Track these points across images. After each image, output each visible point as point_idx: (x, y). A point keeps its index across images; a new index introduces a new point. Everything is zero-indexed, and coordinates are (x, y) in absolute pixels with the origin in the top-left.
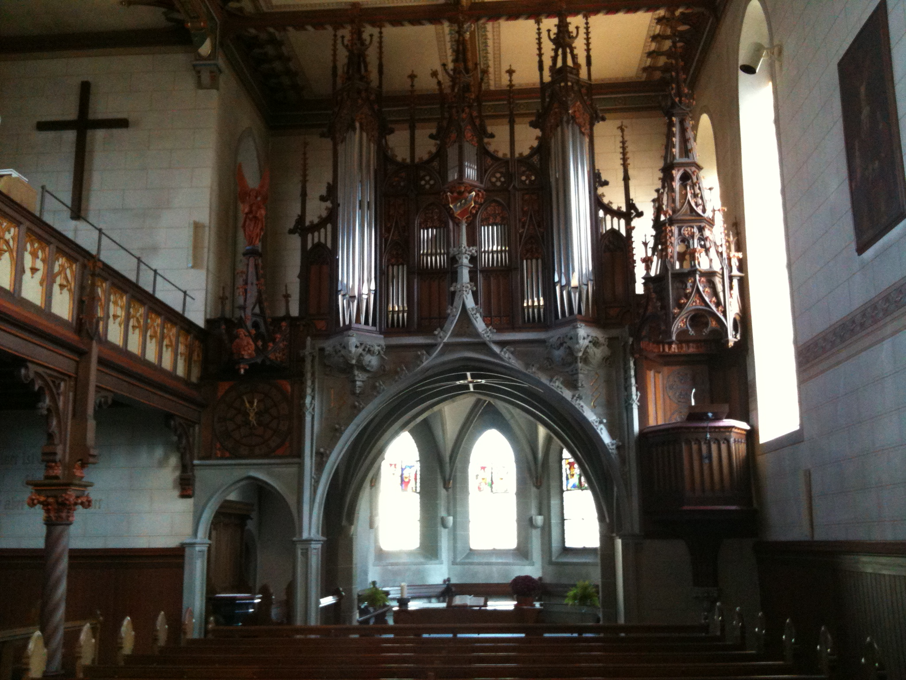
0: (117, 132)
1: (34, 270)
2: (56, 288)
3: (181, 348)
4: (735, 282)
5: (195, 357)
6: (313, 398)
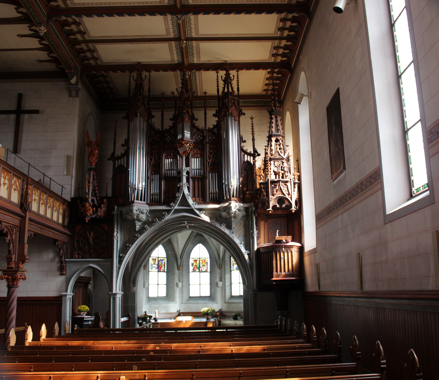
0: (34, 115)
1: (4, 184)
2: (13, 190)
3: (61, 211)
4: (296, 186)
5: (66, 213)
6: (117, 232)
